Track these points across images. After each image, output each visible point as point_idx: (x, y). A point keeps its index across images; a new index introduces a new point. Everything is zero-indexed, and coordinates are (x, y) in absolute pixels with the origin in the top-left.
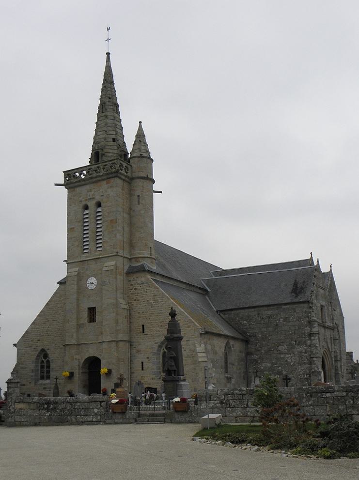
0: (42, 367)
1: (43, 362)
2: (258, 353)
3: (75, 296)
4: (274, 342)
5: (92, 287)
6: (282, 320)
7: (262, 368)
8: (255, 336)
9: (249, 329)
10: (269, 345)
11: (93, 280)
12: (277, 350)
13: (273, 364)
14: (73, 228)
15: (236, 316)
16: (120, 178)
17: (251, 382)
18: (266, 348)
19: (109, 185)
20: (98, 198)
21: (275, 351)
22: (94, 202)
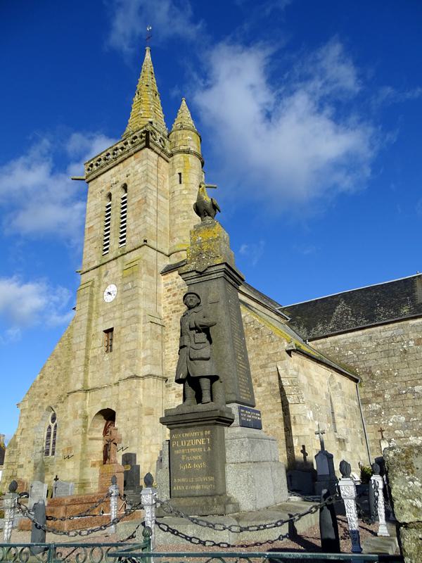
0: (49, 436)
1: (50, 427)
2: (380, 399)
3: (86, 316)
4: (405, 379)
5: (109, 299)
6: (412, 343)
7: (391, 424)
8: (370, 371)
9: (358, 363)
10: (396, 386)
11: (112, 288)
12: (414, 393)
13: (409, 417)
14: (92, 227)
15: (334, 345)
16: (153, 149)
17: (337, 481)
18: (392, 392)
19: (138, 160)
20: (123, 180)
21: (409, 395)
22: (119, 186)
